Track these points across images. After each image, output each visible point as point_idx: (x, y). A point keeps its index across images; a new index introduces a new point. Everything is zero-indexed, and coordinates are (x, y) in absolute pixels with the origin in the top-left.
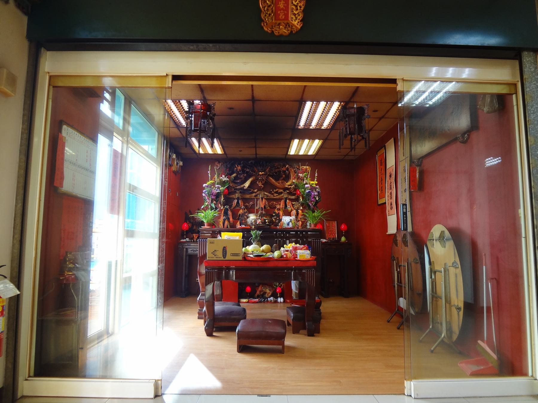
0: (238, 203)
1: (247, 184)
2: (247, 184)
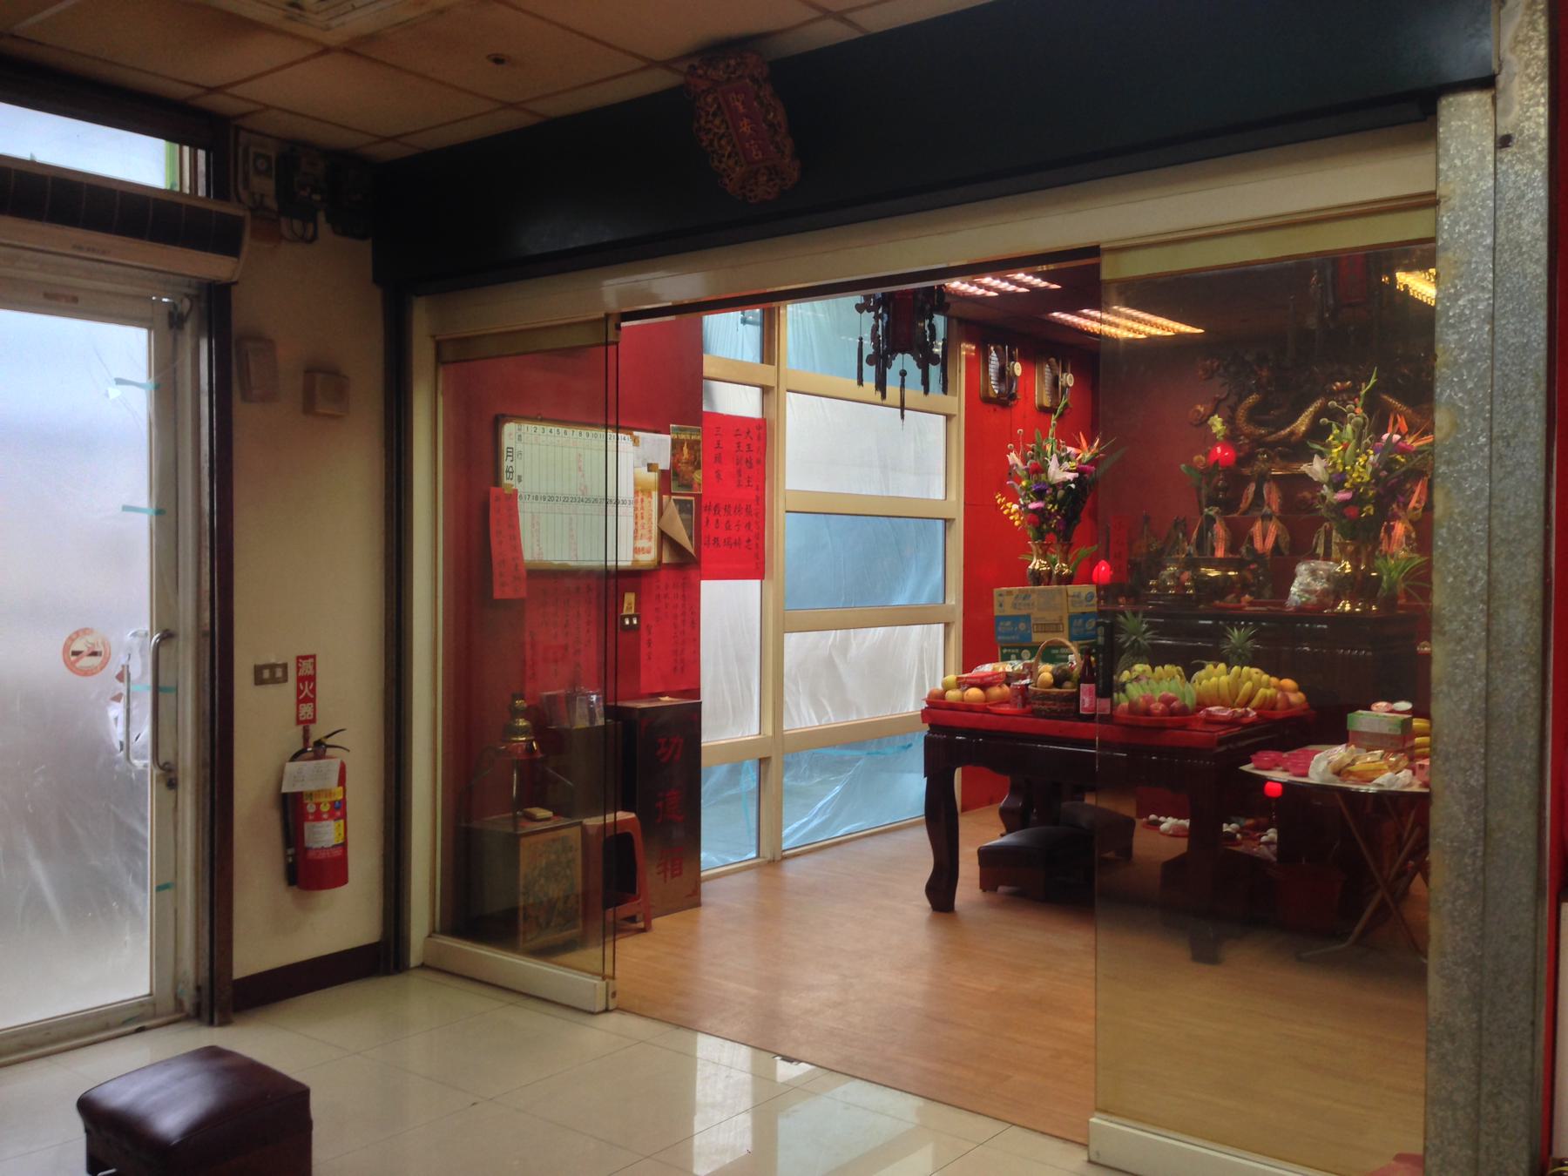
0: (1258, 493)
1: (1302, 424)
2: (1302, 424)
